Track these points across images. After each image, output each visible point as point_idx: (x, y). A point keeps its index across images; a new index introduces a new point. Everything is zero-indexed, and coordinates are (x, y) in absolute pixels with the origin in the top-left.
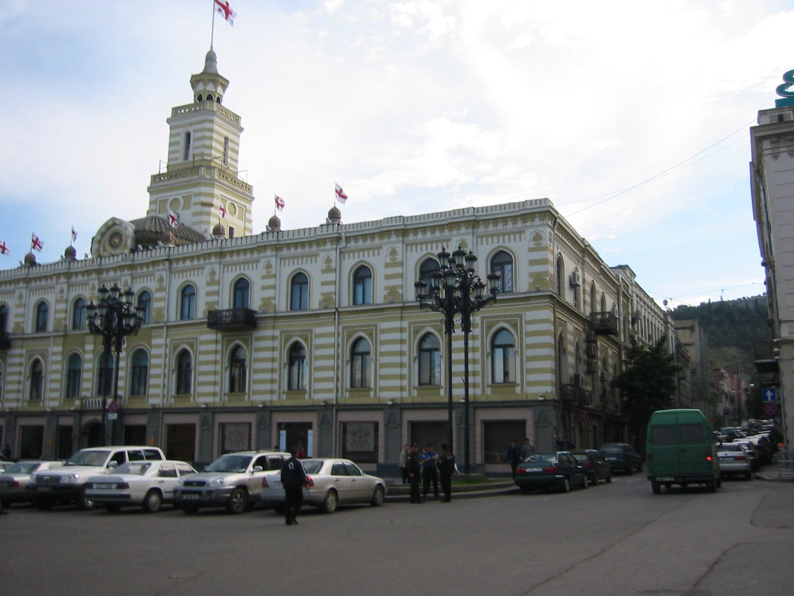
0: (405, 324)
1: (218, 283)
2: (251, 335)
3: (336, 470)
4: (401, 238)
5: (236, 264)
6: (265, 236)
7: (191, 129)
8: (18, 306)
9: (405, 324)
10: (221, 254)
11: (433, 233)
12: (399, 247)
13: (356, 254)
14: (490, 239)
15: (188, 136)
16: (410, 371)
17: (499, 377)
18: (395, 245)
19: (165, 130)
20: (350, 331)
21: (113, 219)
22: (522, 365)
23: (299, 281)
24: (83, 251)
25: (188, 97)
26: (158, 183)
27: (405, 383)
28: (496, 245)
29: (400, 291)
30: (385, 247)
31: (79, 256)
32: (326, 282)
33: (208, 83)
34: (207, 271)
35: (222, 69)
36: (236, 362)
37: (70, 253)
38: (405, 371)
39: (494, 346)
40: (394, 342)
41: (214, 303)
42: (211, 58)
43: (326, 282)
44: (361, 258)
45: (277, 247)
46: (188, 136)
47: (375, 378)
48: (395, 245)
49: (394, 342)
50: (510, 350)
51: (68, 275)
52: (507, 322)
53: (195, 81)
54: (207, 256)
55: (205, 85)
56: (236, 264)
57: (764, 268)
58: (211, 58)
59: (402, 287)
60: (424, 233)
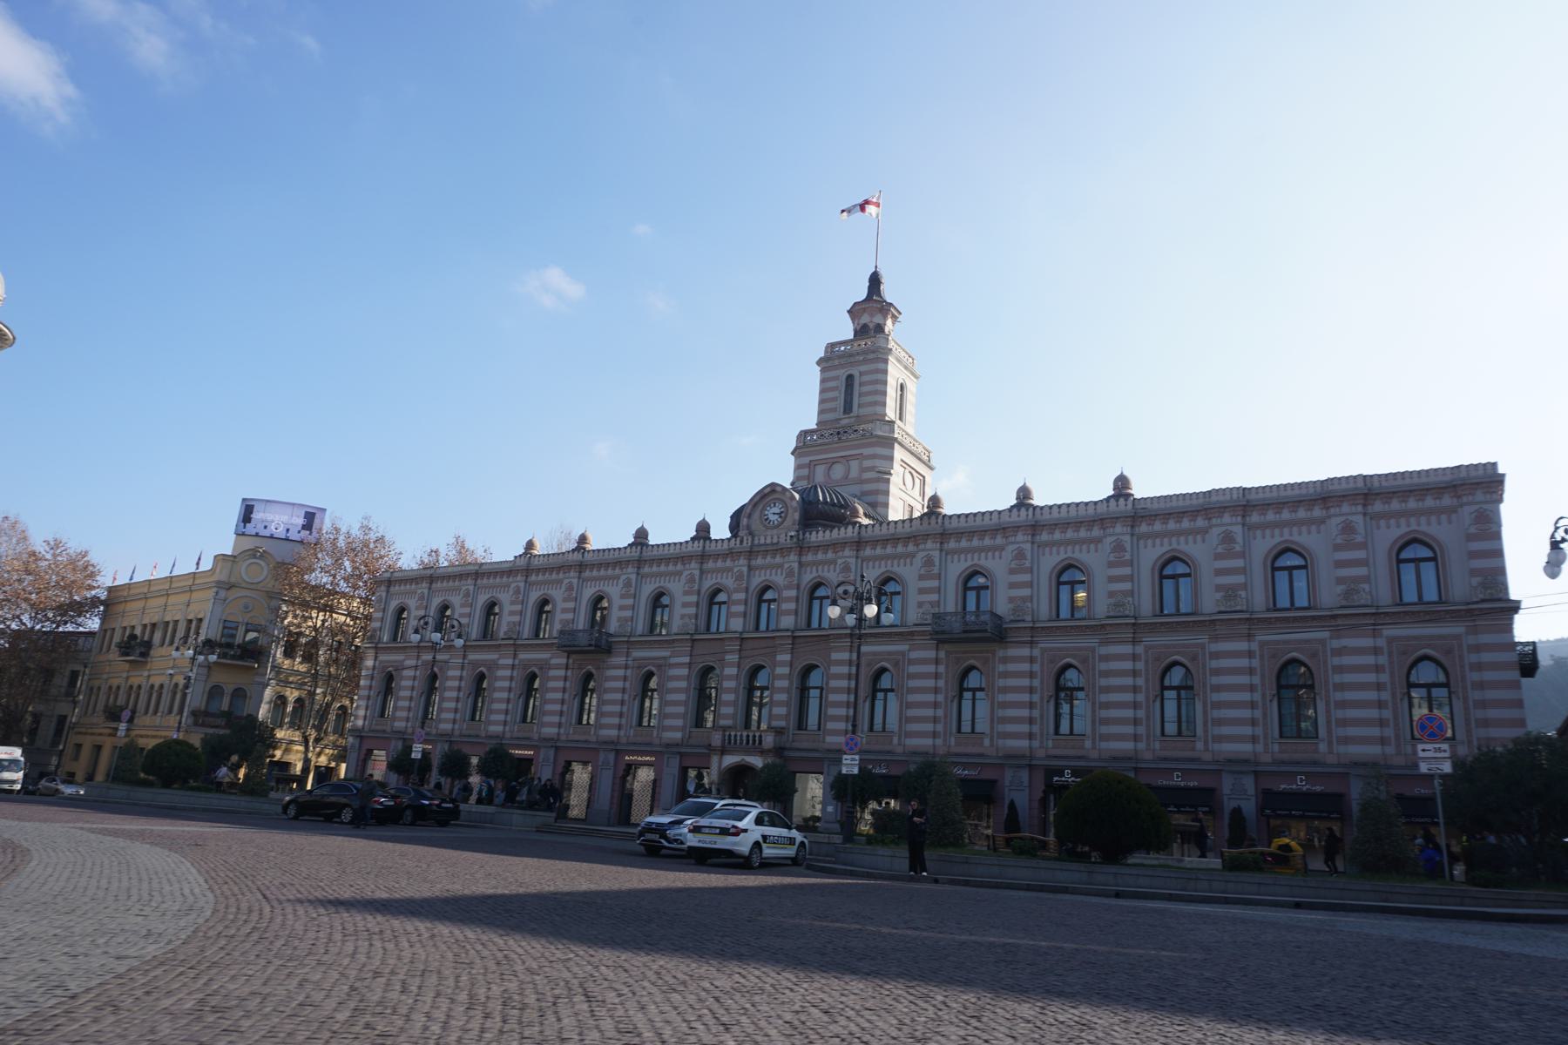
0: (1254, 646)
1: (1031, 571)
3: (759, 821)
5: (1059, 543)
7: (855, 372)
8: (462, 606)
9: (1140, 649)
11: (906, 546)
14: (1158, 541)
15: (850, 378)
16: (1265, 715)
17: (1171, 728)
19: (813, 378)
20: (475, 664)
21: (773, 485)
24: (720, 531)
25: (846, 331)
26: (805, 446)
27: (1141, 730)
29: (1243, 594)
30: (1215, 531)
32: (466, 613)
33: (872, 310)
34: (918, 561)
35: (889, 292)
36: (585, 685)
37: (703, 528)
42: (875, 281)
43: (466, 613)
45: (581, 567)
46: (850, 378)
47: (1205, 723)
51: (703, 557)
52: (1074, 657)
53: (854, 312)
54: (843, 544)
55: (872, 315)
56: (1059, 543)
58: (875, 281)
60: (1179, 521)
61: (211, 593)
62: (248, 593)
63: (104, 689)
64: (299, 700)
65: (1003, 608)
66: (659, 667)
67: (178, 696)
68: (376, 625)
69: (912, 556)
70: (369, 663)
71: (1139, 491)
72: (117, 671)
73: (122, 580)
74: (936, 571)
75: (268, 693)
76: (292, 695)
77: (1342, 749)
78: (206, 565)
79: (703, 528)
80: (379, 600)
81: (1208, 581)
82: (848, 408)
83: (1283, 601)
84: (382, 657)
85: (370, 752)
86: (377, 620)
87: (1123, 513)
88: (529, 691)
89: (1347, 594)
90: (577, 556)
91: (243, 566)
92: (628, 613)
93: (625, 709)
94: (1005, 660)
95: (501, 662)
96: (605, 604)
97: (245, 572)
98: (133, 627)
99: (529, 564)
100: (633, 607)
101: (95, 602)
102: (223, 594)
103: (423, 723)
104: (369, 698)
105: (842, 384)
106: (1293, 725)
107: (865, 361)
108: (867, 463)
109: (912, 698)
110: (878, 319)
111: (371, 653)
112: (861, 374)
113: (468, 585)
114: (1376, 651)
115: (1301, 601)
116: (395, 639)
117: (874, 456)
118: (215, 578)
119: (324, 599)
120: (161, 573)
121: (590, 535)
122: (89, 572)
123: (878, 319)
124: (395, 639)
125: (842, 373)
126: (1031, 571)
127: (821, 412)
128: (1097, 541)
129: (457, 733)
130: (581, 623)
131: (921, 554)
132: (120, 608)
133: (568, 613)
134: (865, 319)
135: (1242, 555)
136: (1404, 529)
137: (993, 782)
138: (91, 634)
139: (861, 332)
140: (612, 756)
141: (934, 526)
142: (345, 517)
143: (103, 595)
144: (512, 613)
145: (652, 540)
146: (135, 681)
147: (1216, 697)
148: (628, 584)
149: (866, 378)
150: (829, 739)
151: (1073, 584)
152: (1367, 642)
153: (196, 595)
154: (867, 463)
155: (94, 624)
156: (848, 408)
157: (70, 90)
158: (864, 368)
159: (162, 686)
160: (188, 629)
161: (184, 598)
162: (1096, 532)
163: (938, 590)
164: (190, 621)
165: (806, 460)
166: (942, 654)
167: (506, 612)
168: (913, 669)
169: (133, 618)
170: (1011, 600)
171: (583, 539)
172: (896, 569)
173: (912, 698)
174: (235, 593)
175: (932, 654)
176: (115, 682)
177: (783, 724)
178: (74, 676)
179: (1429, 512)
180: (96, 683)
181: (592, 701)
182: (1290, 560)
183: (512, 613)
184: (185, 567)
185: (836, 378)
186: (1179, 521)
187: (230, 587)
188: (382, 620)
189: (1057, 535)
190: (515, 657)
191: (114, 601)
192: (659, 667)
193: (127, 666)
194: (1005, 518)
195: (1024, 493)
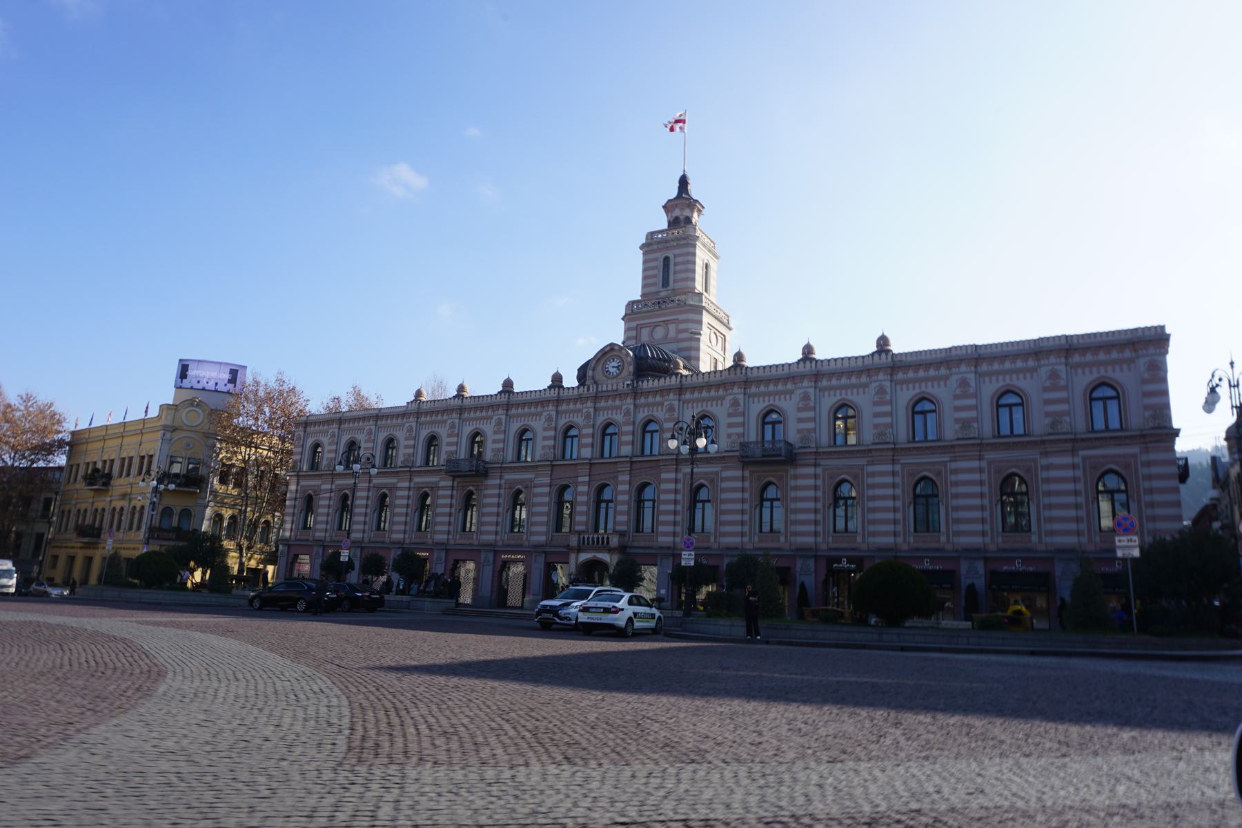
0: (984, 464)
2: (786, 472)
4: (1063, 360)
5: (759, 395)
6: (876, 356)
7: (670, 254)
8: (366, 441)
10: (681, 390)
12: (1062, 369)
13: (1094, 369)
15: (666, 259)
18: (968, 376)
19: (639, 256)
20: (378, 487)
22: (947, 514)
23: (390, 443)
24: (570, 381)
25: (660, 222)
26: (633, 313)
28: (838, 397)
31: (566, 384)
33: (682, 206)
35: (694, 191)
37: (557, 379)
38: (899, 516)
39: (762, 500)
40: (885, 486)
41: (452, 453)
42: (684, 182)
44: (844, 396)
45: (461, 410)
46: (666, 259)
47: (1039, 520)
48: (968, 376)
49: (885, 486)
50: (610, 505)
51: (558, 401)
55: (682, 210)
56: (998, 373)
57: (1175, 425)
58: (684, 182)
59: (891, 425)
60: (927, 370)
61: (160, 434)
63: (74, 512)
64: (233, 517)
65: (793, 437)
67: (137, 516)
71: (897, 347)
72: (84, 498)
73: (83, 425)
74: (888, 397)
75: (208, 512)
76: (227, 513)
77: (871, 540)
79: (557, 379)
81: (949, 415)
82: (665, 283)
83: (1005, 430)
85: (296, 557)
87: (885, 364)
88: (422, 507)
89: (1053, 425)
90: (458, 402)
94: (796, 477)
95: (400, 485)
98: (95, 463)
101: (61, 443)
102: (168, 435)
105: (660, 264)
106: (925, 524)
107: (678, 246)
108: (682, 326)
110: (687, 213)
112: (675, 256)
113: (334, 428)
114: (1074, 467)
115: (1019, 429)
117: (687, 321)
118: (162, 422)
119: (246, 437)
120: (117, 419)
122: (55, 419)
123: (687, 213)
125: (660, 256)
126: (891, 403)
127: (644, 286)
128: (865, 386)
129: (500, 543)
131: (799, 392)
132: (83, 447)
134: (677, 213)
135: (975, 396)
136: (1095, 375)
137: (789, 568)
138: (60, 468)
139: (674, 223)
141: (739, 376)
142: (263, 371)
146: (100, 505)
147: (954, 502)
149: (679, 259)
150: (661, 539)
152: (976, 464)
154: (682, 326)
155: (61, 460)
156: (665, 283)
158: (677, 251)
161: (137, 439)
162: (721, 392)
164: (143, 457)
165: (634, 324)
166: (747, 473)
167: (444, 443)
168: (725, 485)
169: (94, 455)
170: (799, 431)
171: (461, 388)
174: (177, 435)
175: (739, 473)
176: (83, 507)
177: (625, 528)
178: (48, 502)
179: (853, 386)
180: (67, 508)
181: (472, 516)
182: (927, 406)
184: (136, 415)
185: (656, 259)
187: (174, 429)
189: (834, 382)
191: (76, 442)
192: (526, 487)
193: (92, 493)
194: (794, 369)
195: (883, 342)
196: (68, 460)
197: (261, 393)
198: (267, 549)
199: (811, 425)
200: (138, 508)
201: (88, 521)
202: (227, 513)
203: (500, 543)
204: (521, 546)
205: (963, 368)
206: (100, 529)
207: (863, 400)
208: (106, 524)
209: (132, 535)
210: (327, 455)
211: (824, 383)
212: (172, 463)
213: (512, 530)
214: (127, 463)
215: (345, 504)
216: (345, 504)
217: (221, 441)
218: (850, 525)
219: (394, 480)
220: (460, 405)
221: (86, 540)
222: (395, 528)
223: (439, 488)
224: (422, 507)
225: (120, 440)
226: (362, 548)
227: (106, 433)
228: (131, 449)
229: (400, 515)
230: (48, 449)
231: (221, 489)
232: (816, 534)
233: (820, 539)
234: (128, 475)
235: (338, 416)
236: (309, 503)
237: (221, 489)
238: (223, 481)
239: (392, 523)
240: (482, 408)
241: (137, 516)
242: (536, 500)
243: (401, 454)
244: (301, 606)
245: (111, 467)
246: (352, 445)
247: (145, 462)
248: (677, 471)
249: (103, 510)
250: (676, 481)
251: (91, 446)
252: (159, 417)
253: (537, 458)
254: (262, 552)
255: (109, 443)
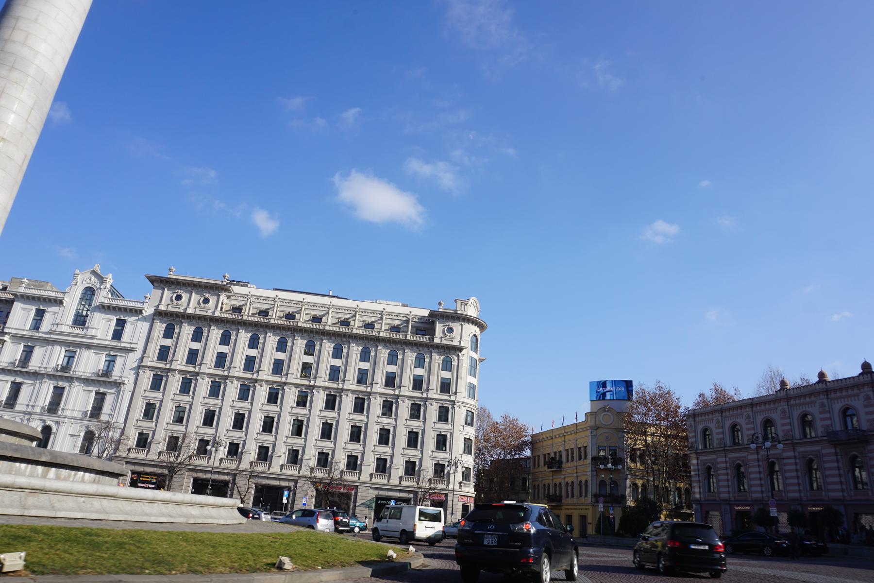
5: (840, 398)
8: (747, 424)
60: (853, 390)
61: (589, 433)
62: (605, 430)
63: (541, 486)
64: (643, 485)
65: (865, 426)
66: (777, 459)
67: (569, 488)
68: (693, 440)
69: (858, 395)
70: (694, 462)
72: (546, 476)
73: (537, 431)
74: (827, 409)
75: (628, 482)
76: (640, 483)
78: (582, 418)
80: (691, 426)
84: (701, 458)
85: (708, 512)
86: (692, 437)
87: (786, 396)
88: (771, 472)
90: (782, 394)
91: (601, 416)
92: (721, 436)
93: (800, 481)
95: (719, 460)
96: (809, 418)
97: (602, 419)
98: (549, 454)
99: (787, 394)
100: (790, 424)
101: (525, 443)
102: (594, 432)
103: (772, 495)
104: (699, 481)
109: (827, 473)
111: (693, 457)
116: (705, 447)
118: (589, 424)
119: (641, 429)
120: (558, 425)
121: (825, 371)
122: (522, 430)
124: (705, 447)
126: (829, 412)
129: (732, 499)
130: (838, 426)
131: (780, 408)
132: (540, 445)
133: (825, 419)
138: (528, 458)
140: (728, 507)
142: (645, 382)
143: (528, 439)
144: (718, 434)
145: (830, 378)
146: (557, 481)
148: (718, 422)
151: (852, 416)
153: (579, 435)
155: (527, 453)
157: (420, 208)
159: (572, 483)
160: (580, 453)
161: (574, 436)
162: (856, 391)
163: (830, 419)
164: (580, 448)
166: (838, 451)
167: (714, 434)
168: (825, 459)
169: (548, 449)
170: (868, 421)
172: (850, 403)
173: (827, 473)
174: (600, 431)
176: (547, 482)
178: (524, 480)
180: (536, 483)
181: (714, 480)
183: (718, 434)
184: (570, 421)
186: (853, 390)
187: (597, 428)
188: (695, 437)
189: (838, 394)
190: (794, 450)
191: (535, 442)
192: (777, 459)
193: (551, 474)
194: (856, 380)
196: (532, 453)
197: (648, 398)
198: (669, 507)
199: (828, 422)
200: (583, 482)
201: (552, 492)
202: (640, 483)
203: (732, 499)
204: (715, 500)
205: (866, 389)
206: (561, 496)
207: (814, 411)
208: (564, 493)
209: (583, 500)
210: (746, 433)
211: (792, 402)
212: (599, 450)
213: (856, 488)
214: (570, 453)
215: (739, 474)
216: (739, 474)
217: (628, 433)
218: (779, 485)
219: (714, 457)
220: (824, 389)
221: (554, 504)
222: (754, 489)
223: (718, 463)
224: (771, 472)
225: (562, 439)
226: (730, 505)
227: (553, 434)
228: (571, 443)
229: (723, 480)
230: (520, 448)
231: (632, 465)
232: (800, 491)
233: (765, 495)
234: (572, 460)
235: (719, 407)
236: (708, 472)
237: (632, 465)
238: (633, 461)
239: (750, 486)
240: (847, 388)
241: (569, 488)
242: (827, 465)
243: (716, 437)
244: (768, 551)
245: (560, 456)
246: (768, 423)
247: (582, 452)
248: (794, 450)
249: (560, 484)
250: (726, 462)
251: (545, 443)
252: (586, 421)
253: (820, 434)
254: (667, 510)
255: (556, 441)
